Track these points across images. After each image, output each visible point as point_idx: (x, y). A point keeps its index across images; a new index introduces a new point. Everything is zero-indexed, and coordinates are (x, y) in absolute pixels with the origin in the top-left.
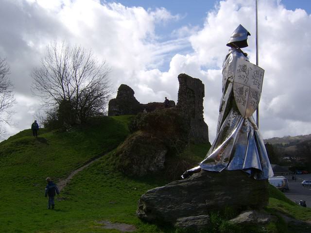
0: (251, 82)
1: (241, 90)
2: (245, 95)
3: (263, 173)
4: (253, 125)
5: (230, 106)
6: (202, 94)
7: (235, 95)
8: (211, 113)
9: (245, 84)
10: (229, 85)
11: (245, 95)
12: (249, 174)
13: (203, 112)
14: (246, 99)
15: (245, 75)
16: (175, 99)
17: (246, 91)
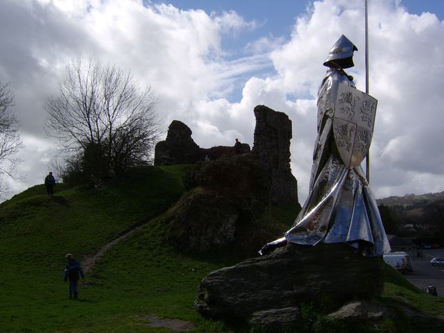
0: (358, 117)
1: (344, 128)
2: (350, 135)
3: (376, 247)
4: (361, 179)
5: (328, 152)
6: (289, 135)
7: (335, 136)
8: (302, 162)
9: (349, 119)
10: (328, 121)
11: (350, 135)
12: (355, 249)
13: (290, 161)
14: (352, 141)
15: (350, 107)
16: (250, 141)
17: (351, 130)
